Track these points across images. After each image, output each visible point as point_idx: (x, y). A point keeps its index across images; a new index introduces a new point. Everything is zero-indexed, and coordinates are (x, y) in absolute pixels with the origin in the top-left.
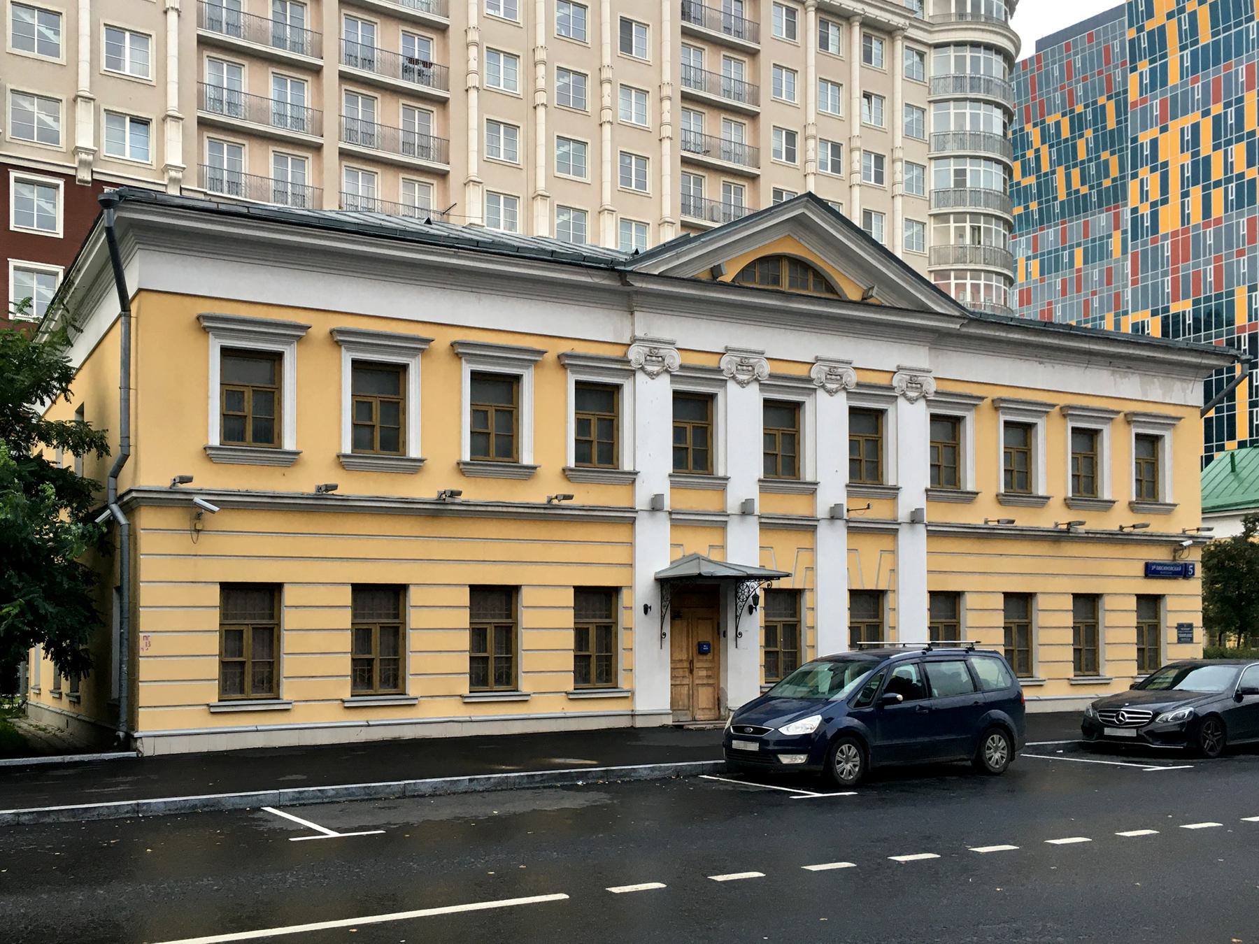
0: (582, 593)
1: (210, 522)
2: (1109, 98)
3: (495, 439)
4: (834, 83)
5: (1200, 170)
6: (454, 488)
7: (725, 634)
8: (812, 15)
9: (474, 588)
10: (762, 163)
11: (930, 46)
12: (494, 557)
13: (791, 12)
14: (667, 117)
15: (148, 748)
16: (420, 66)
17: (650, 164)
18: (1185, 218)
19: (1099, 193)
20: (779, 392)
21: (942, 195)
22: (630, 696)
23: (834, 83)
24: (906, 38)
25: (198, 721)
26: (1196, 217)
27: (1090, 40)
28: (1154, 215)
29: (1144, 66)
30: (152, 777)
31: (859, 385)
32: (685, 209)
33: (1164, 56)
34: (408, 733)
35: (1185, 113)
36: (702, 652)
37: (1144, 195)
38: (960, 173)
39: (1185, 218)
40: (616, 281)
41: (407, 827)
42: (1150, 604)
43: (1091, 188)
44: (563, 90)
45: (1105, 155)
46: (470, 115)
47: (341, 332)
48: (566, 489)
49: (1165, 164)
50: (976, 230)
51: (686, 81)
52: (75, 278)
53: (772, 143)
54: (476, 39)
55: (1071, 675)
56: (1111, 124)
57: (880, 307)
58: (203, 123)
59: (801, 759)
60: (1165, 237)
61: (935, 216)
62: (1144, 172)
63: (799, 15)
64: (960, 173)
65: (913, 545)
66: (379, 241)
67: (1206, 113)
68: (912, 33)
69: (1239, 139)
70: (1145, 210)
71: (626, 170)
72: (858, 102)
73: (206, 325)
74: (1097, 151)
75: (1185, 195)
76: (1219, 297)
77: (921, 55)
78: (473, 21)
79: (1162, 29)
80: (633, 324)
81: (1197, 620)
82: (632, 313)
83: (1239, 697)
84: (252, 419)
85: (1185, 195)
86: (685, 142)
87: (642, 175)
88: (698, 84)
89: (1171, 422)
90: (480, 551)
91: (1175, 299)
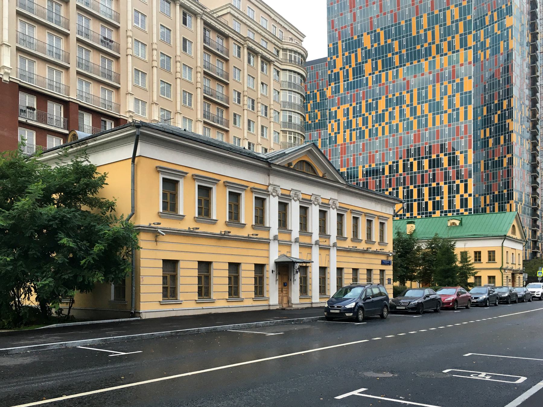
0: (166, 262)
1: (161, 238)
2: (318, 91)
3: (205, 209)
4: (252, 77)
5: (349, 124)
6: (197, 227)
7: (291, 280)
8: (246, 50)
9: (164, 261)
10: (230, 103)
11: (281, 69)
12: (206, 251)
13: (239, 48)
14: (199, 80)
15: (144, 316)
16: (108, 41)
17: (193, 96)
18: (345, 140)
19: (314, 124)
20: (174, 177)
21: (284, 123)
22: (268, 300)
23: (252, 77)
24: (274, 65)
25: (156, 307)
26: (348, 141)
27: (312, 69)
28: (336, 137)
29: (333, 85)
30: (125, 327)
31: (282, 194)
32: (205, 116)
33: (339, 83)
34: (213, 311)
35: (345, 104)
36: (285, 286)
37: (333, 130)
38: (290, 117)
39: (345, 140)
40: (267, 166)
41: (291, 331)
42: (382, 271)
43: (312, 122)
44: (163, 61)
45: (316, 111)
46: (128, 66)
47: (196, 176)
48: (158, 220)
49: (339, 120)
50: (295, 138)
51: (205, 67)
52: (90, 142)
53: (234, 96)
54: (131, 35)
55: (197, 298)
56: (318, 100)
57: (298, 171)
58: (18, 50)
59: (351, 314)
60: (339, 145)
61: (282, 131)
62: (333, 121)
63: (242, 49)
64: (290, 117)
65: (333, 252)
66: (201, 144)
67: (351, 105)
68: (276, 64)
69: (360, 116)
70: (333, 135)
71: (185, 98)
72: (260, 85)
73: (159, 170)
74: (314, 109)
75: (345, 132)
76: (354, 168)
77: (278, 72)
78: (130, 27)
79: (338, 73)
80: (269, 179)
81: (392, 278)
82: (269, 176)
83: (425, 298)
84: (170, 204)
85: (345, 132)
86: (205, 90)
87: (190, 101)
88: (209, 69)
89: (387, 219)
90: (228, 251)
91: (342, 167)
